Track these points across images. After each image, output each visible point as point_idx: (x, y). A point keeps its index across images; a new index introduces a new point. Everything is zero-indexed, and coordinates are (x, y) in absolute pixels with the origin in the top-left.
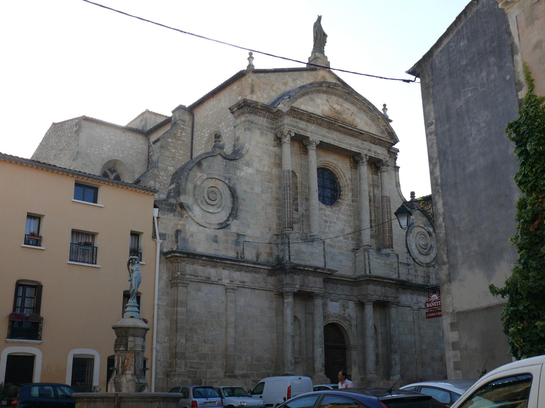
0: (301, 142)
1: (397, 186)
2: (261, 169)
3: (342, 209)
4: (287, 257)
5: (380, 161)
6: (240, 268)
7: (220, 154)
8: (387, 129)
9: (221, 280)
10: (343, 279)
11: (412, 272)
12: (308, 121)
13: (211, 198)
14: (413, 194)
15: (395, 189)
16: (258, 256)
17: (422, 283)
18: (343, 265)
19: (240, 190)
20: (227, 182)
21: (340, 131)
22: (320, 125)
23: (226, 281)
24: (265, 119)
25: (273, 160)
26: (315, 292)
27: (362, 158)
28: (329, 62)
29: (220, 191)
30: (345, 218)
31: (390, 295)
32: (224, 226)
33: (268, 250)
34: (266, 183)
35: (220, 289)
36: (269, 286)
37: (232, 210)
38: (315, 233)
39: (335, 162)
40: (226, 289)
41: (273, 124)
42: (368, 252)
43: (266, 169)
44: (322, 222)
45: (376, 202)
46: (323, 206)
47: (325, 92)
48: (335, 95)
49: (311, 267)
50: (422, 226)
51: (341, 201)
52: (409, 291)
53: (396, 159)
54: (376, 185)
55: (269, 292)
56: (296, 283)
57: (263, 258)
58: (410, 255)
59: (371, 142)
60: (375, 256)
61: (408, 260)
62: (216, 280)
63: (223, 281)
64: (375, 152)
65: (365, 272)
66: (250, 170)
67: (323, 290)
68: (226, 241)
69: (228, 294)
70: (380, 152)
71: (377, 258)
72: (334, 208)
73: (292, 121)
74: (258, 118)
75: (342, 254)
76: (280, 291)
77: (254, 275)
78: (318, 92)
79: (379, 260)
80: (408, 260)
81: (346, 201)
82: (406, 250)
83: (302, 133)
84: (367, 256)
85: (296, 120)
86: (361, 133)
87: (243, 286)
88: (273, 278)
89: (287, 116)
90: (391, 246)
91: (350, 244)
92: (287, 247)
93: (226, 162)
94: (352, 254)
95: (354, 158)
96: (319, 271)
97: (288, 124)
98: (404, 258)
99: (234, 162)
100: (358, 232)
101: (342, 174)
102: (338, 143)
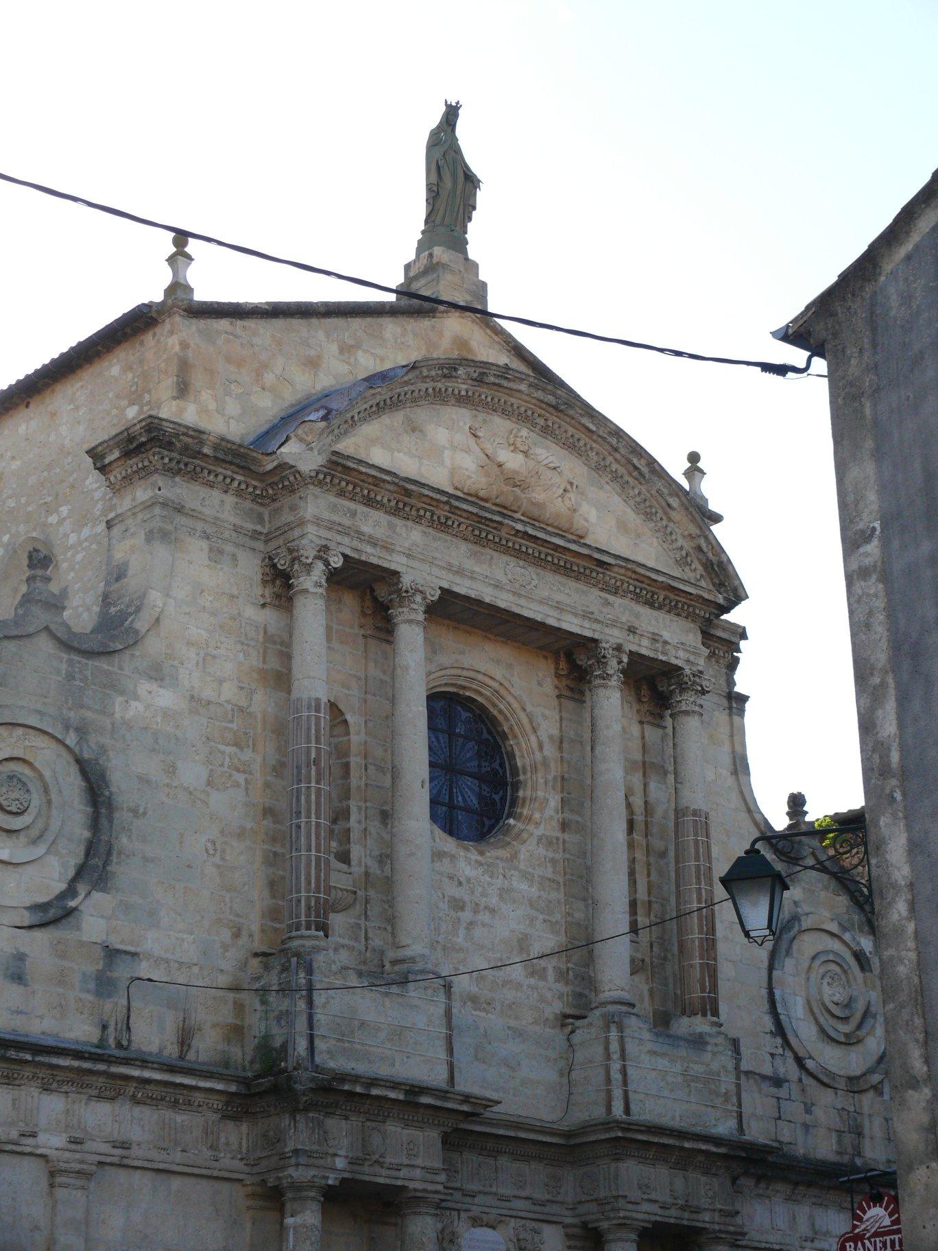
1: (735, 772)
2: (208, 693)
4: (302, 1046)
5: (671, 671)
7: (47, 628)
8: (699, 548)
9: (34, 1135)
10: (523, 1135)
12: (396, 512)
14: (796, 803)
15: (730, 781)
17: (832, 1158)
18: (522, 1080)
20: (71, 740)
21: (518, 554)
23: (52, 1142)
24: (230, 499)
26: (412, 1185)
27: (601, 661)
31: (704, 1203)
32: (54, 914)
33: (226, 1015)
34: (229, 750)
36: (228, 1162)
37: (87, 854)
39: (498, 673)
40: (52, 1174)
41: (260, 519)
42: (621, 1029)
43: (229, 692)
44: (444, 906)
45: (655, 830)
46: (449, 844)
47: (463, 400)
49: (395, 1085)
50: (834, 927)
51: (520, 826)
52: (779, 1186)
53: (733, 664)
55: (225, 1187)
56: (335, 1147)
57: (206, 1047)
58: (787, 1043)
59: (637, 597)
60: (649, 1046)
61: (778, 1061)
62: (14, 1135)
63: (42, 1138)
64: (655, 638)
66: (165, 698)
69: (60, 1193)
70: (674, 639)
71: (653, 1053)
72: (492, 854)
73: (334, 508)
74: (203, 492)
75: (519, 1033)
77: (168, 1114)
79: (662, 1063)
80: (778, 1061)
81: (537, 824)
83: (372, 555)
84: (614, 1046)
85: (352, 505)
87: (121, 1159)
88: (244, 1128)
90: (710, 1007)
91: (552, 995)
92: (302, 1005)
94: (559, 1036)
95: (574, 661)
97: (318, 521)
98: (760, 1053)
99: (103, 664)
100: (581, 947)
101: (525, 721)
102: (511, 598)
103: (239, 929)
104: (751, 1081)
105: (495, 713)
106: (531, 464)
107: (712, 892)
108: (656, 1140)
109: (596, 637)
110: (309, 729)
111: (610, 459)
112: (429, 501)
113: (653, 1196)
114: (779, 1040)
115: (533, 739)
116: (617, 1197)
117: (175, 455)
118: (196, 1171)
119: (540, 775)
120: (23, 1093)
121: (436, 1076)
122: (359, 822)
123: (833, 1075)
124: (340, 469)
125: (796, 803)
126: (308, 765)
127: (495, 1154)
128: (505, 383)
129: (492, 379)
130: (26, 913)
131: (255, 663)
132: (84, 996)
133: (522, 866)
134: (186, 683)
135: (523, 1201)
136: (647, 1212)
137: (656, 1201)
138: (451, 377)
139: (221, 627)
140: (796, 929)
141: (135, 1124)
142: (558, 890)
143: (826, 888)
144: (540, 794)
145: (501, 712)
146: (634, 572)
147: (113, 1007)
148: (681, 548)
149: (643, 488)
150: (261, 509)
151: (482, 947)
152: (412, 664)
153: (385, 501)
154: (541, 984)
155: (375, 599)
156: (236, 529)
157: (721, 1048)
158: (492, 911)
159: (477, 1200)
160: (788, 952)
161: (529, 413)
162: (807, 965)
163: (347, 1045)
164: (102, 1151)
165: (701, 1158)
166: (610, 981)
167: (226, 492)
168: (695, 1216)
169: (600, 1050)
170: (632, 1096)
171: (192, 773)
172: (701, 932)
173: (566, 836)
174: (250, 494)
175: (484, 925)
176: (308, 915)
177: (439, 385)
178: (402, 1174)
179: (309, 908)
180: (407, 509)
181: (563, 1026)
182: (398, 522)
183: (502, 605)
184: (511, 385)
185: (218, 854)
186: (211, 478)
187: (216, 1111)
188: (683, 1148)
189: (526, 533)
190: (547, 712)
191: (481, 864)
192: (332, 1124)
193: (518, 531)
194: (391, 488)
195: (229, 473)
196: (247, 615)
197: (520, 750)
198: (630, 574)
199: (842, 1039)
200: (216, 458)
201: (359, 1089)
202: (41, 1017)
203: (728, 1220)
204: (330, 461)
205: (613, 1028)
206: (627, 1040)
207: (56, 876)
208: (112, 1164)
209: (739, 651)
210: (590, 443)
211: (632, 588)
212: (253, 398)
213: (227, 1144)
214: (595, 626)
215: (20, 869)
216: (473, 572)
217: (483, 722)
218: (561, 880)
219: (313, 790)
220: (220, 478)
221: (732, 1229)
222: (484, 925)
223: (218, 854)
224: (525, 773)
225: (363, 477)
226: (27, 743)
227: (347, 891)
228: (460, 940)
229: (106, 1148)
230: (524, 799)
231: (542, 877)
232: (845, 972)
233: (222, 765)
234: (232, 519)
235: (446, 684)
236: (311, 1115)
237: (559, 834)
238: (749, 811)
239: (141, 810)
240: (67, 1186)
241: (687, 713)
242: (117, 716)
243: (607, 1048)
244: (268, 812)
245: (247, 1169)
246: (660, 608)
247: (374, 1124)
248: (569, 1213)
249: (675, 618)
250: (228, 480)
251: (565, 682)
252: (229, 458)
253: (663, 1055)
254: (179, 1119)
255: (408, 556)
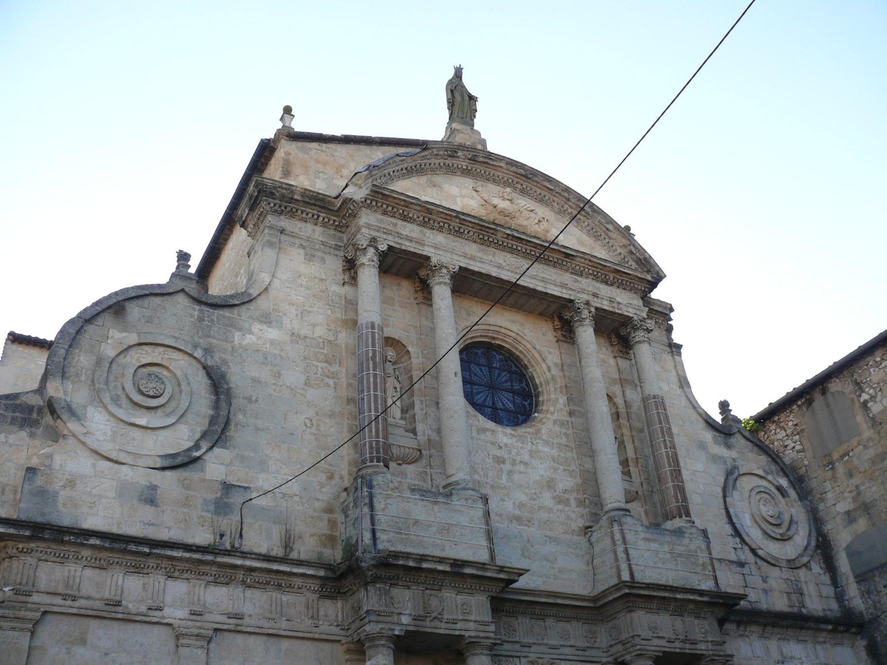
0: (404, 268)
1: (681, 387)
2: (305, 331)
3: (544, 430)
4: (367, 536)
5: (626, 321)
6: (226, 575)
8: (631, 252)
9: (160, 609)
10: (560, 601)
11: (755, 580)
12: (424, 224)
13: (150, 392)
14: (724, 406)
15: (679, 391)
16: (288, 546)
17: (786, 609)
18: (555, 566)
19: (238, 377)
20: (198, 353)
21: (512, 251)
22: (458, 233)
23: (176, 614)
24: (319, 229)
25: (339, 314)
26: (467, 634)
27: (578, 311)
28: (484, 141)
29: (175, 375)
30: (555, 452)
31: (699, 637)
32: (183, 462)
33: (322, 527)
35: (157, 639)
36: (325, 628)
38: (460, 476)
39: (515, 328)
40: (177, 638)
41: (341, 240)
42: (621, 525)
43: (320, 331)
44: (489, 461)
45: (633, 416)
47: (466, 172)
48: (494, 181)
49: (441, 560)
51: (541, 415)
52: (754, 628)
53: (670, 329)
54: (632, 379)
55: (327, 647)
57: (305, 549)
58: (743, 541)
59: (596, 278)
60: (643, 535)
61: (739, 552)
62: (143, 609)
63: (167, 611)
64: (611, 300)
65: (619, 576)
66: (272, 333)
67: (492, 628)
68: (186, 503)
69: (183, 651)
70: (626, 303)
71: (646, 540)
74: (300, 224)
76: (356, 638)
77: (275, 594)
78: (450, 170)
79: (654, 546)
80: (739, 552)
81: (552, 413)
82: (729, 529)
84: (618, 536)
85: (394, 220)
86: (567, 255)
87: (235, 625)
88: (339, 604)
89: (368, 211)
90: (684, 511)
91: (577, 517)
92: (366, 510)
93: (201, 311)
94: (583, 541)
95: (560, 315)
96: (468, 571)
97: (369, 226)
98: (724, 545)
99: (226, 313)
100: (591, 483)
101: (537, 355)
102: (510, 274)
103: (332, 474)
104: (723, 564)
105: (518, 353)
106: (515, 207)
107: (673, 442)
108: (655, 594)
109: (572, 298)
110: (367, 339)
111: (566, 206)
112: (444, 216)
113: (661, 634)
114: (738, 540)
115: (544, 366)
116: (633, 637)
117: (277, 201)
118: (300, 635)
119: (551, 385)
120: (151, 579)
121: (483, 556)
122: (422, 409)
123: (777, 559)
124: (380, 196)
125: (724, 406)
126: (368, 360)
127: (543, 617)
128: (491, 162)
129: (482, 159)
130: (159, 460)
131: (339, 315)
132: (205, 514)
133: (544, 437)
134: (289, 325)
135: (568, 649)
136: (658, 645)
137: (663, 638)
138: (454, 157)
139: (314, 296)
140: (736, 474)
141: (253, 603)
142: (572, 451)
143: (752, 451)
144: (552, 396)
145: (521, 352)
146: (590, 261)
147: (228, 523)
148: (620, 254)
149: (590, 221)
150: (342, 235)
151: (521, 486)
152: (443, 307)
153: (415, 217)
154: (566, 509)
155: (419, 278)
156: (323, 243)
157: (695, 536)
158: (526, 464)
159: (532, 649)
160: (734, 487)
161: (510, 181)
162: (747, 495)
163: (404, 536)
164: (219, 621)
165: (691, 606)
166: (610, 497)
167: (316, 224)
168: (693, 646)
169: (608, 541)
170: (634, 568)
171: (294, 377)
172: (670, 466)
173: (573, 419)
174: (332, 225)
175: (521, 473)
176: (371, 453)
177: (447, 162)
178: (458, 626)
179: (371, 448)
180: (431, 222)
181: (585, 534)
182: (425, 230)
183: (505, 278)
184: (494, 163)
185: (315, 426)
186: (304, 215)
187: (314, 592)
188: (676, 599)
189: (513, 236)
190: (551, 350)
191: (514, 436)
192: (396, 592)
193: (508, 235)
194: (417, 208)
195: (315, 212)
196: (332, 289)
197: (537, 374)
198: (587, 262)
199: (779, 537)
200: (305, 202)
201: (411, 564)
202: (169, 528)
203: (719, 647)
204: (372, 191)
205: (615, 525)
206: (626, 531)
207: (186, 437)
208: (230, 631)
209: (671, 319)
210: (552, 198)
211: (591, 272)
212: (335, 180)
213: (326, 616)
214: (570, 292)
215: (157, 432)
216: (481, 258)
217: (511, 361)
218: (573, 446)
219: (371, 376)
220: (310, 215)
221: (722, 653)
222: (521, 473)
223: (315, 426)
224: (541, 386)
225: (396, 201)
226: (166, 356)
227: (413, 449)
228: (504, 481)
229: (224, 619)
230: (543, 402)
231: (560, 444)
232: (773, 498)
233: (316, 373)
234: (321, 239)
235: (481, 336)
236: (378, 586)
237: (568, 419)
238: (694, 408)
239: (254, 398)
240: (189, 646)
241: (639, 342)
242: (236, 342)
243: (613, 538)
244: (349, 401)
245: (343, 633)
246: (612, 285)
247: (432, 592)
248: (605, 655)
249: (623, 291)
250: (316, 217)
251: (560, 333)
252: (313, 202)
253: (654, 541)
254: (285, 598)
255: (435, 248)
